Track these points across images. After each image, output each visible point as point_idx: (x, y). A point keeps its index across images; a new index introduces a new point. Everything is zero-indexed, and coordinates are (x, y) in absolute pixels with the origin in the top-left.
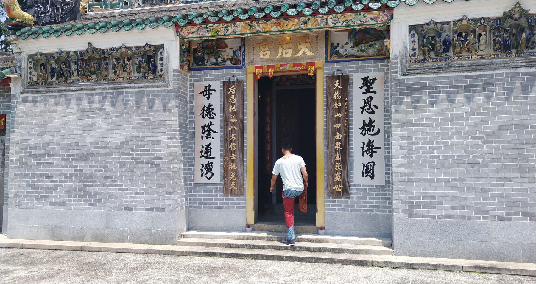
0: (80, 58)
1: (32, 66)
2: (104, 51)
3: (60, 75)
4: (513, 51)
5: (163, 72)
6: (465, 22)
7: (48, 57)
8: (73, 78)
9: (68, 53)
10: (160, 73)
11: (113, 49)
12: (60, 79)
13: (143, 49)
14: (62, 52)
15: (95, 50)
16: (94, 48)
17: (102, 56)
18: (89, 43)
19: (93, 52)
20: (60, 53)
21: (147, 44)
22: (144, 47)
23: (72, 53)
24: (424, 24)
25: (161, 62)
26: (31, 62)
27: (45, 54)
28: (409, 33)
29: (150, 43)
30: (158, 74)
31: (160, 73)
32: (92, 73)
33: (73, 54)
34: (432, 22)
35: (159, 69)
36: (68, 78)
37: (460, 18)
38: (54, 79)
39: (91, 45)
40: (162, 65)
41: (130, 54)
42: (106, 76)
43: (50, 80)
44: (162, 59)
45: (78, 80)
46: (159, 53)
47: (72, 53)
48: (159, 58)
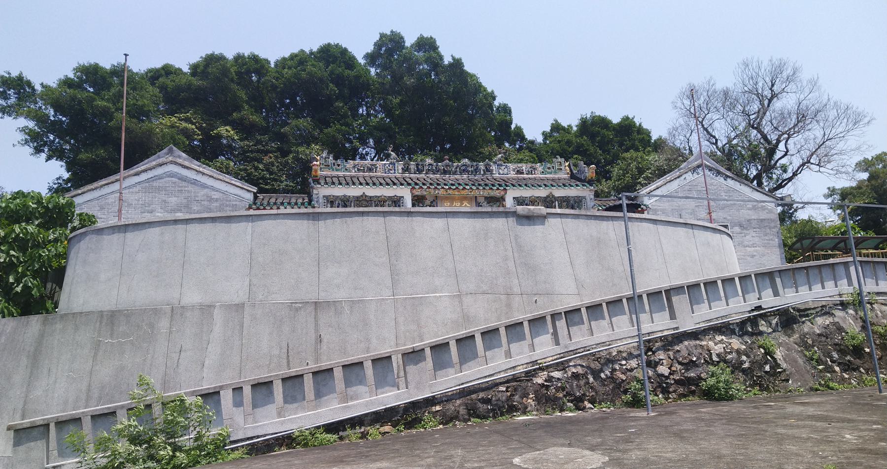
2: (371, 197)
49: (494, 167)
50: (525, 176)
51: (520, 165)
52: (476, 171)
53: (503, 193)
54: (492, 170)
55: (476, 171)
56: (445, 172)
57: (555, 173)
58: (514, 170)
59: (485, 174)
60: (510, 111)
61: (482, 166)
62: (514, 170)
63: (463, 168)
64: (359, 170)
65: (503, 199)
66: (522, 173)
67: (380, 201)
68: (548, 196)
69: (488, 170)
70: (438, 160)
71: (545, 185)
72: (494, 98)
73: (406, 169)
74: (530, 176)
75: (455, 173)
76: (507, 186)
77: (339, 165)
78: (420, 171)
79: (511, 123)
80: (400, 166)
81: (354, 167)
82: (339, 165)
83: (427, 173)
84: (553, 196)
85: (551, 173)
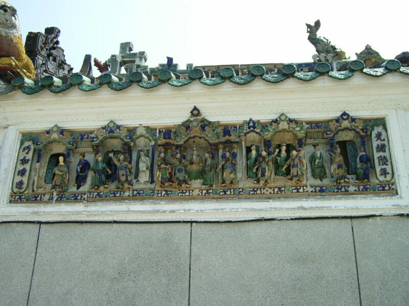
0: (162, 141)
1: (29, 156)
2: (227, 130)
3: (104, 178)
4: (197, 184)
5: (389, 177)
6: (284, 125)
7: (77, 138)
8: (136, 186)
9: (132, 131)
10: (382, 178)
11: (252, 125)
12: (102, 188)
13: (333, 126)
14: (119, 127)
15: (205, 124)
16: (203, 120)
17: (223, 139)
18: (195, 108)
19: (203, 128)
20: (111, 129)
21: (344, 114)
22: (337, 120)
23: (140, 131)
24: (331, 121)
25: (381, 154)
26: (28, 148)
27: (72, 133)
28: (22, 143)
29: (353, 114)
30: (374, 181)
31: (382, 178)
32: (191, 176)
33: (144, 132)
34: (283, 118)
35: (378, 169)
36: (126, 185)
37: (274, 117)
38: (85, 188)
39: (199, 114)
40: (384, 160)
41: (301, 134)
42: (232, 183)
43: (73, 189)
44: (382, 148)
45: (153, 191)
46: (374, 135)
47: (140, 131)
48: (375, 145)
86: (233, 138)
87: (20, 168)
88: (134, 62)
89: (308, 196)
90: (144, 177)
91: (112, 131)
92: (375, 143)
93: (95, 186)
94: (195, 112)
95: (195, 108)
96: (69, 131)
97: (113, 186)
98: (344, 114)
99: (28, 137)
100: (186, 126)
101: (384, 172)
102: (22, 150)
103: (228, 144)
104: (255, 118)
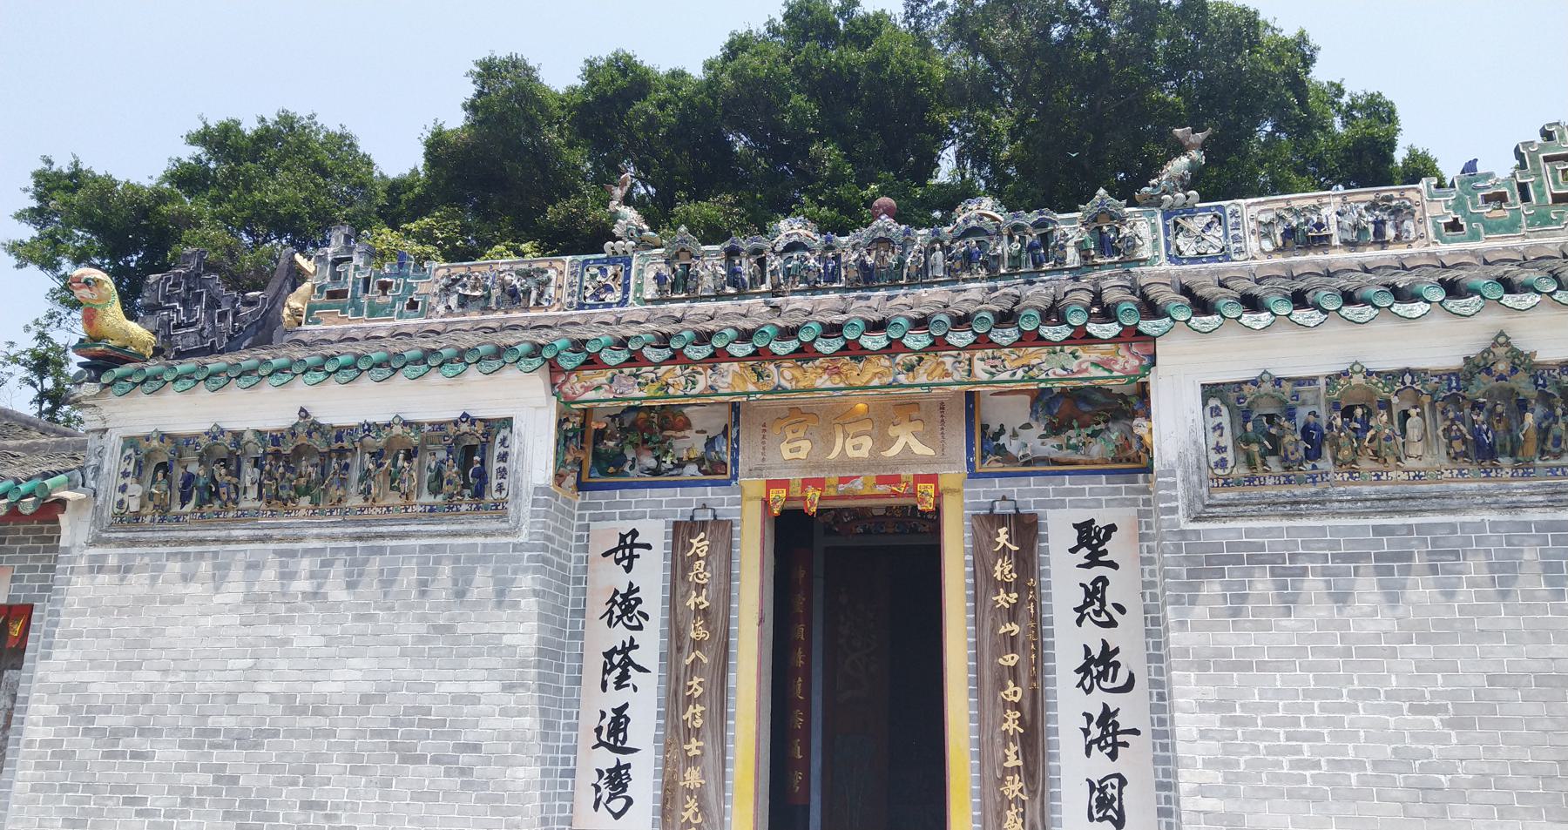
0: (270, 449)
1: (131, 468)
2: (340, 433)
3: (206, 495)
7: (180, 444)
9: (237, 436)
10: (496, 495)
11: (368, 428)
12: (205, 508)
13: (451, 429)
15: (315, 428)
17: (335, 446)
18: (302, 410)
19: (309, 434)
20: (215, 434)
21: (465, 415)
22: (456, 423)
23: (248, 436)
25: (502, 465)
26: (129, 457)
29: (473, 414)
30: (488, 498)
32: (301, 492)
36: (230, 504)
38: (189, 507)
39: (307, 415)
42: (340, 501)
43: (176, 509)
44: (503, 457)
45: (258, 510)
49: (1143, 227)
50: (1338, 256)
51: (1300, 200)
52: (1042, 250)
53: (1127, 360)
54: (1132, 243)
55: (1041, 252)
56: (868, 278)
57: (1542, 220)
58: (1265, 230)
59: (1087, 264)
60: (1392, 112)
61: (1070, 228)
62: (1265, 230)
63: (959, 248)
64: (464, 301)
65: (1135, 402)
66: (1320, 241)
67: (390, 455)
68: (1476, 367)
69: (1108, 244)
70: (845, 216)
71: (1453, 289)
72: (1308, 61)
73: (681, 283)
74: (1371, 254)
75: (921, 277)
76: (1151, 309)
77: (384, 287)
78: (738, 286)
79: (1392, 145)
80: (648, 269)
81: (447, 290)
82: (384, 287)
83: (776, 292)
84: (1520, 362)
85: (1511, 226)
86: (346, 444)
87: (121, 482)
88: (351, 259)
89: (415, 518)
90: (253, 493)
91: (215, 438)
92: (498, 450)
93: (200, 505)
94: (304, 412)
95: (302, 410)
96: (170, 436)
97: (217, 505)
98: (465, 415)
99: (131, 442)
100: (293, 431)
101: (500, 488)
102: (1500, 271)
103: (341, 452)
104: (370, 420)
